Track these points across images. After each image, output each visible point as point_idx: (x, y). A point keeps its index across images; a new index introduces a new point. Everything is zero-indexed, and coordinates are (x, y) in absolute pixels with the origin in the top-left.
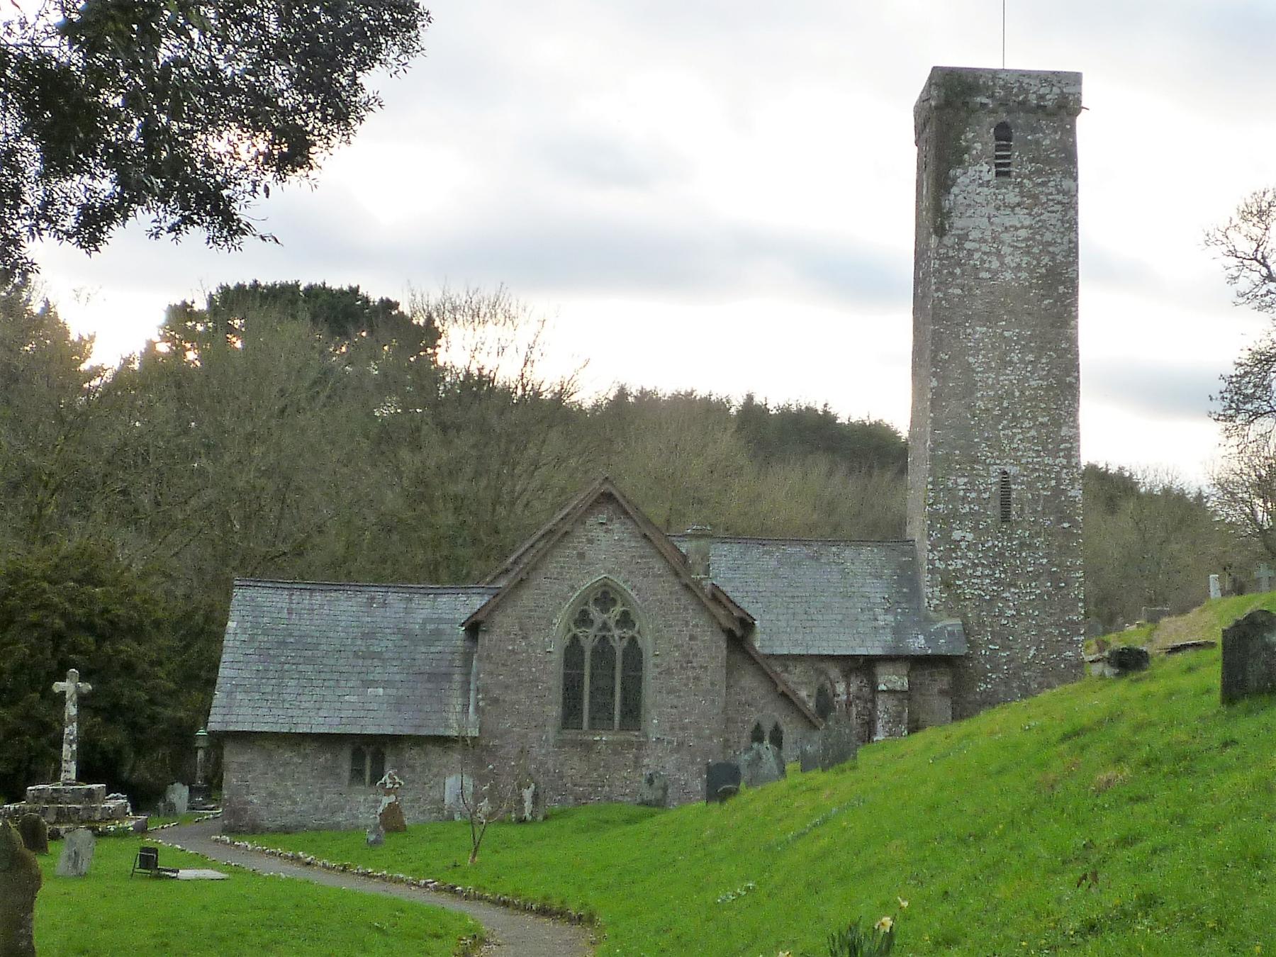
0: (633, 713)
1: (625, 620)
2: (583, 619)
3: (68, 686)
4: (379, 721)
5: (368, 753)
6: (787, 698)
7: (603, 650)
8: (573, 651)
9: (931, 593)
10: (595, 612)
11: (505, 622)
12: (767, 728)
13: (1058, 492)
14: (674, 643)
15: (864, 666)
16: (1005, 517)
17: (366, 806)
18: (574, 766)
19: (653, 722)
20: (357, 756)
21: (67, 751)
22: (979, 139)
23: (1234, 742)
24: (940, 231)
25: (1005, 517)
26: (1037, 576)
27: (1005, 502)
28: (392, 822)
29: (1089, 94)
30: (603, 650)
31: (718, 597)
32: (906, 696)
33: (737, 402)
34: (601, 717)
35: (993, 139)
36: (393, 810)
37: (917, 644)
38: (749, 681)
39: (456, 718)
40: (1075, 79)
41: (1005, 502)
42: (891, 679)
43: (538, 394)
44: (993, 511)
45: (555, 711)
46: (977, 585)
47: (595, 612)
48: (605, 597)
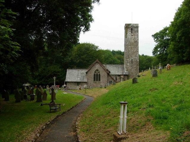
0: (100, 80)
1: (99, 72)
2: (95, 72)
3: (55, 78)
4: (78, 80)
5: (78, 83)
6: (113, 79)
7: (97, 75)
8: (95, 75)
9: (125, 69)
10: (96, 72)
11: (89, 72)
12: (111, 81)
13: (137, 60)
14: (103, 74)
15: (119, 76)
16: (132, 63)
17: (78, 87)
18: (95, 84)
19: (101, 80)
20: (77, 83)
21: (55, 83)
22: (129, 30)
23: (157, 89)
24: (126, 38)
25: (132, 63)
26: (135, 68)
27: (132, 61)
28: (80, 89)
29: (139, 26)
30: (97, 75)
31: (107, 70)
32: (123, 78)
33: (112, 51)
34: (97, 80)
35: (131, 29)
36: (80, 88)
37: (124, 74)
38: (109, 77)
39: (85, 80)
40: (138, 24)
41: (132, 61)
42: (122, 77)
43: (180, 8)
44: (131, 62)
45: (93, 80)
46: (130, 68)
47: (96, 72)
48: (97, 70)
